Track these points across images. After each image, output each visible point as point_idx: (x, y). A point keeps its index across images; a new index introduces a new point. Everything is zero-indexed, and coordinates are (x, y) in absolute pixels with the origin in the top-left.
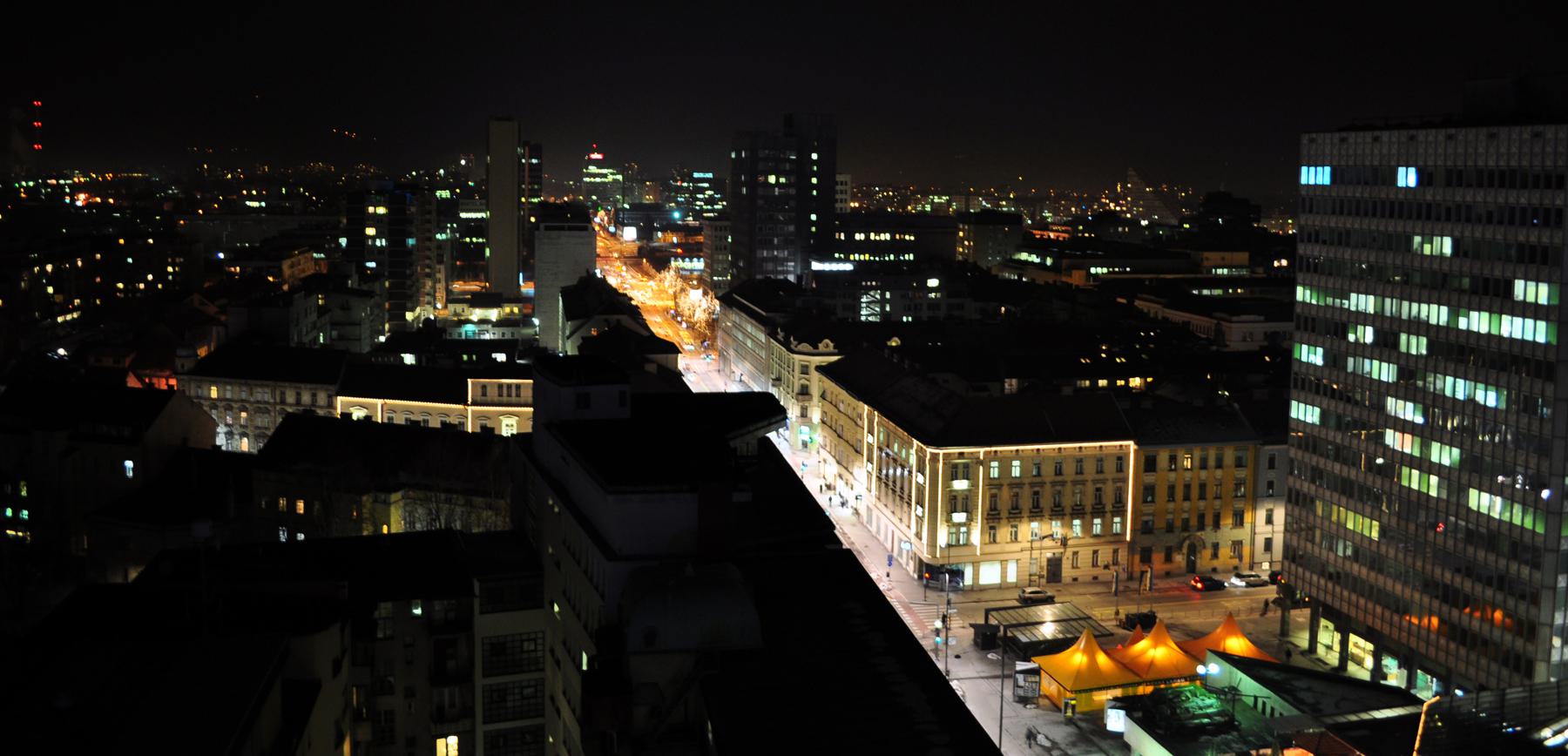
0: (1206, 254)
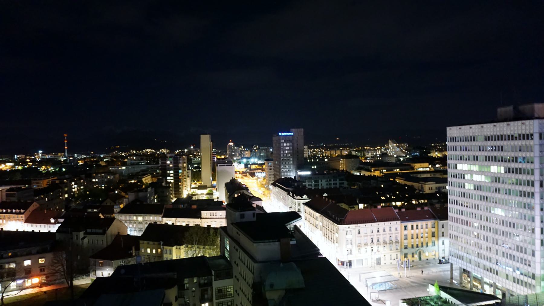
0: (416, 164)
